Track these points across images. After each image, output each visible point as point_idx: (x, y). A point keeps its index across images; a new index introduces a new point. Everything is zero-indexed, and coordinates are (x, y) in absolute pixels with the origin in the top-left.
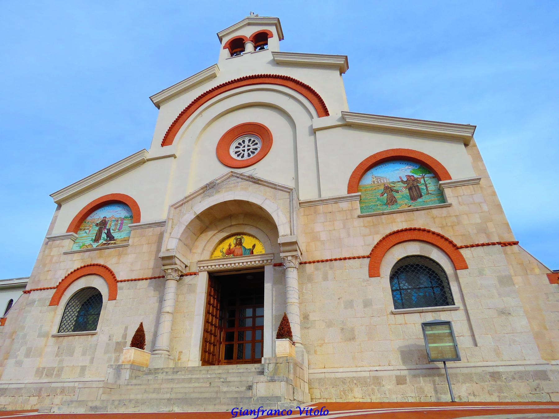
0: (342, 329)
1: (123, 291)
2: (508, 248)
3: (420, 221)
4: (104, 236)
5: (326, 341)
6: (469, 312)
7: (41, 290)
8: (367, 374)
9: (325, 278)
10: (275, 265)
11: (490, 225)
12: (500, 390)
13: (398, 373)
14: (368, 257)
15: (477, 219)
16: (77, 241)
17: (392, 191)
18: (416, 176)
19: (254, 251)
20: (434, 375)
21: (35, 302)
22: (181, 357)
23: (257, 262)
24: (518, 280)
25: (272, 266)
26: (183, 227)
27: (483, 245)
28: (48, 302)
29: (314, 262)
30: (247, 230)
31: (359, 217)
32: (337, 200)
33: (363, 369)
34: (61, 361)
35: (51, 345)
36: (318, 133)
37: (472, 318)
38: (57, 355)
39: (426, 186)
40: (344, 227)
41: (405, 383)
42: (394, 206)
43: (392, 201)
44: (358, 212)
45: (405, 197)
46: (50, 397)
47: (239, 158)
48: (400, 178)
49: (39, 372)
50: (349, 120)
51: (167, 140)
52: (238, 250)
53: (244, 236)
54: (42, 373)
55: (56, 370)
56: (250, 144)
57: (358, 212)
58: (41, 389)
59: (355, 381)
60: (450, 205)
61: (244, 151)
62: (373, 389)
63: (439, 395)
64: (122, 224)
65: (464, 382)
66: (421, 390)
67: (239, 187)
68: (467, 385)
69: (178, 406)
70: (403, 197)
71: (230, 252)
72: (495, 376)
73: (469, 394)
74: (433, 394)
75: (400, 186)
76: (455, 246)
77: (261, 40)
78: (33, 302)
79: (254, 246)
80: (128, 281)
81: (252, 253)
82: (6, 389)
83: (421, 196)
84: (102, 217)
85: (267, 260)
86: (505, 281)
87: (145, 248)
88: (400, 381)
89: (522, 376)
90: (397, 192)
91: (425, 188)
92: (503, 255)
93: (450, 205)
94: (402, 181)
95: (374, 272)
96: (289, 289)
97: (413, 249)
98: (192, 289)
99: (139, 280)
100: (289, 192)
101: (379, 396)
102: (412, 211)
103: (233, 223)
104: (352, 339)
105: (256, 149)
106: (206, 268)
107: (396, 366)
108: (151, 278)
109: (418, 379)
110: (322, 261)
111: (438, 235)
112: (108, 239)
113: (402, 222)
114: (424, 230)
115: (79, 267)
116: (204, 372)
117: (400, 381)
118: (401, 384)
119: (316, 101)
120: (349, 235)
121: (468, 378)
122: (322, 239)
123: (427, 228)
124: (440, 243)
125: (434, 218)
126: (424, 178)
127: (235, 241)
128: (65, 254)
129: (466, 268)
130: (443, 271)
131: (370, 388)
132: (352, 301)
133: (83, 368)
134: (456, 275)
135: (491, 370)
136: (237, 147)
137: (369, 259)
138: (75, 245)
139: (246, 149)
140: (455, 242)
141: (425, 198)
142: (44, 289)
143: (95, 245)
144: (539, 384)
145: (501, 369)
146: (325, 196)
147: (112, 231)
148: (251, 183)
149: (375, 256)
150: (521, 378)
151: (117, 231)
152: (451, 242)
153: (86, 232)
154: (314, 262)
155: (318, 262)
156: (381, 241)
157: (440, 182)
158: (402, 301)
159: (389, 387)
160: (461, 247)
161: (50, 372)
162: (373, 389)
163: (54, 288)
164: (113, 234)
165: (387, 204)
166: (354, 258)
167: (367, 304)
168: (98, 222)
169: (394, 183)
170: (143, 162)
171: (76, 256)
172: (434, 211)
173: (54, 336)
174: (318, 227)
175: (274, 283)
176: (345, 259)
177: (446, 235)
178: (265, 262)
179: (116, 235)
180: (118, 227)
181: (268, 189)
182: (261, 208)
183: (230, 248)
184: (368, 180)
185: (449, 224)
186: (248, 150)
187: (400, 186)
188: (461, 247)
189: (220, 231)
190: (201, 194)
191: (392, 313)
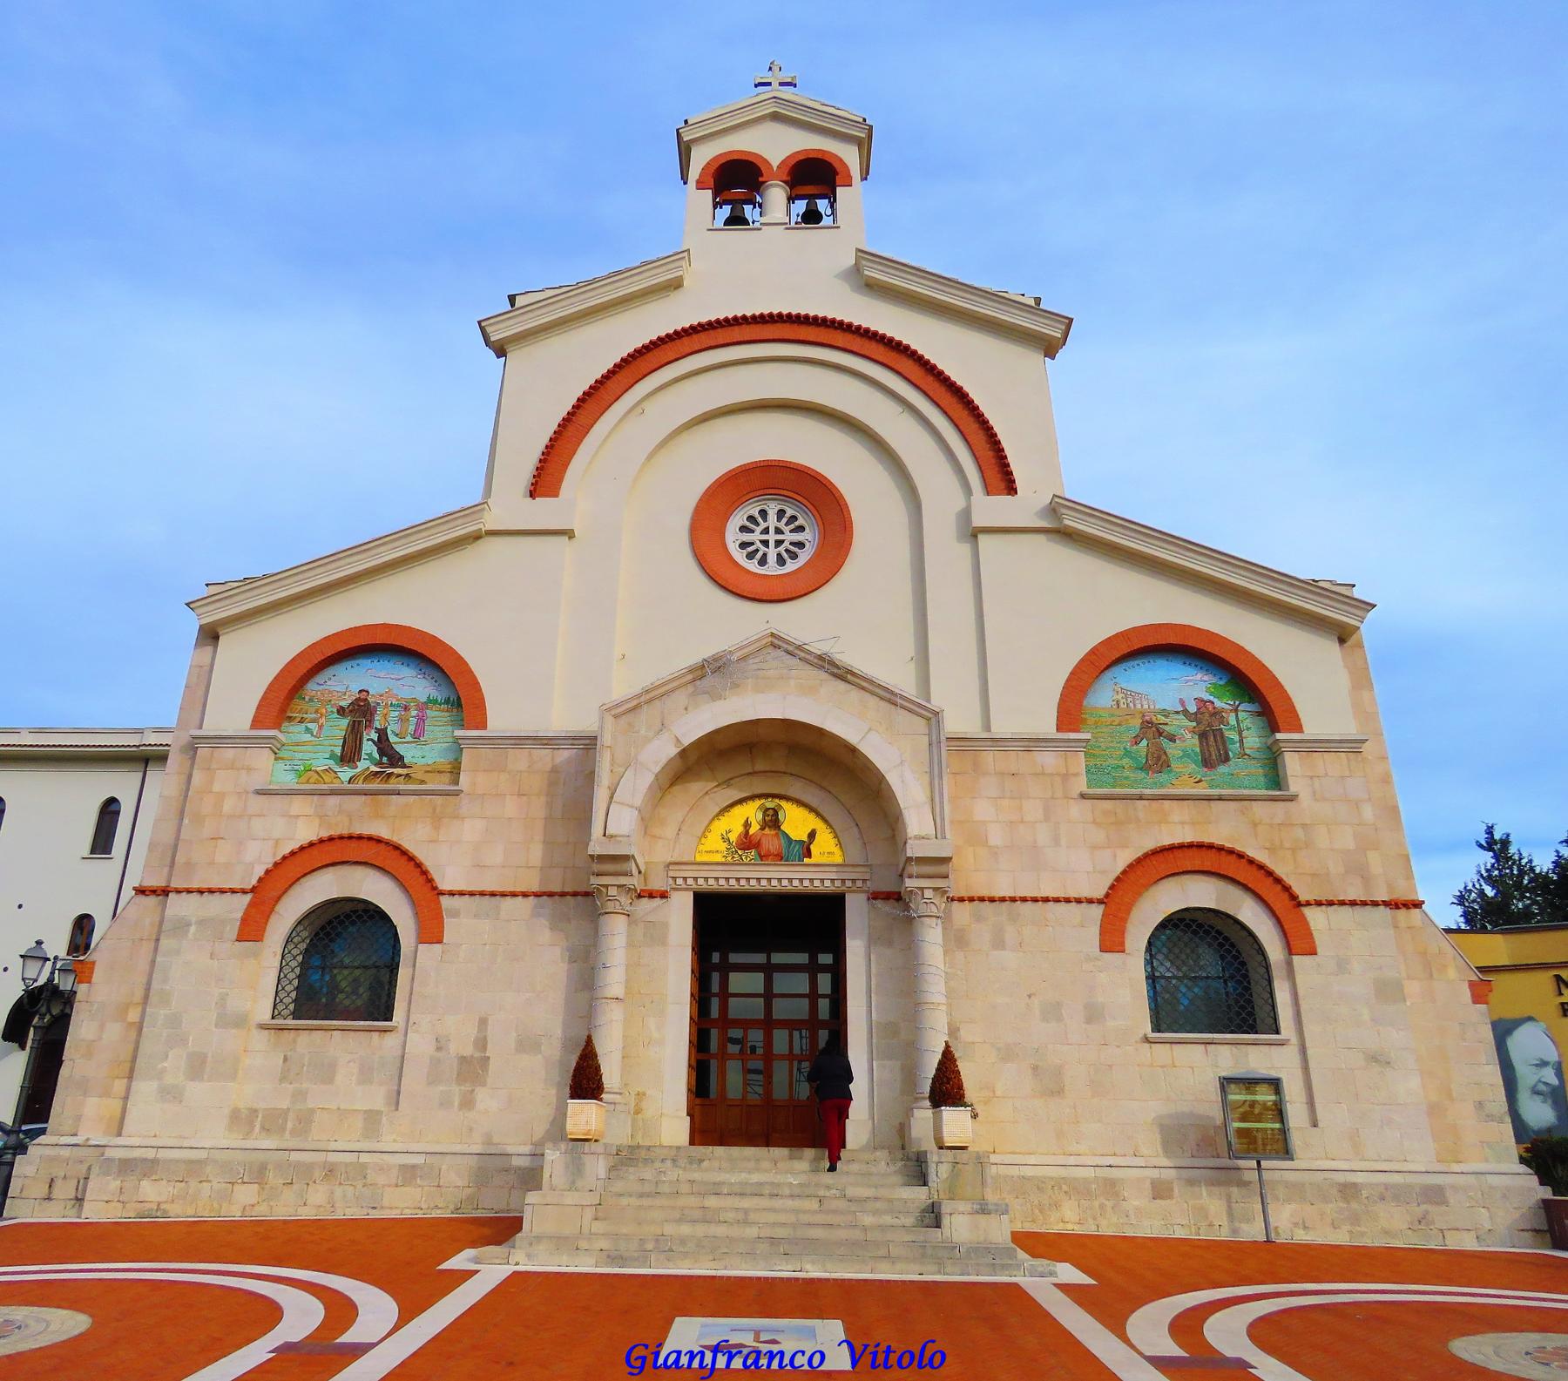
0: (1035, 1068)
1: (460, 921)
2: (1402, 912)
3: (1224, 827)
4: (369, 748)
5: (998, 1093)
6: (1309, 1052)
7: (201, 892)
8: (1089, 1173)
9: (999, 943)
10: (875, 896)
11: (1373, 858)
12: (1355, 1219)
13: (1155, 1173)
14: (1100, 902)
15: (1346, 840)
16: (281, 754)
17: (1160, 734)
18: (1218, 703)
19: (822, 853)
20: (1228, 1183)
21: (189, 925)
22: (644, 1105)
23: (828, 883)
24: (1413, 988)
25: (863, 897)
26: (650, 778)
27: (1353, 903)
28: (232, 930)
29: (971, 899)
30: (796, 788)
31: (1083, 796)
32: (1033, 743)
33: (1079, 1160)
34: (300, 1095)
35: (260, 1055)
36: (983, 539)
37: (1312, 1064)
38: (283, 1079)
39: (1240, 733)
40: (1047, 818)
41: (1170, 1197)
42: (1163, 777)
43: (1158, 762)
44: (1081, 784)
45: (1188, 756)
46: (295, 1187)
47: (752, 566)
48: (1182, 702)
49: (241, 1119)
50: (1070, 522)
51: (545, 480)
52: (771, 842)
53: (783, 803)
54: (251, 1124)
55: (291, 1116)
56: (782, 525)
57: (1081, 784)
58: (263, 1168)
59: (1065, 1188)
60: (1292, 798)
61: (765, 543)
62: (1102, 1206)
63: (1237, 1224)
64: (421, 719)
65: (1288, 1200)
66: (1202, 1212)
67: (792, 682)
68: (1293, 1206)
69: (813, 1263)
70: (1186, 755)
71: (747, 842)
72: (1349, 1191)
73: (1296, 1225)
74: (1225, 1223)
75: (1178, 725)
76: (1293, 897)
77: (815, 179)
78: (182, 926)
79: (812, 835)
80: (472, 894)
81: (809, 854)
82: (155, 1161)
83: (1227, 759)
84: (355, 688)
85: (854, 881)
86: (1388, 991)
87: (511, 807)
88: (1160, 1191)
89: (1395, 1194)
90: (1172, 739)
91: (1237, 738)
92: (1392, 932)
93: (1292, 798)
94: (1185, 712)
95: (1112, 940)
96: (926, 969)
97: (1200, 893)
98: (657, 934)
99: (503, 895)
100: (929, 719)
101: (1114, 1220)
102: (1209, 799)
103: (759, 766)
104: (1059, 1092)
105: (800, 545)
106: (690, 881)
107: (1149, 1158)
108: (537, 895)
109: (1196, 1189)
110: (992, 900)
111: (1261, 867)
112: (385, 759)
113: (1183, 823)
114: (1231, 852)
115: (314, 838)
116: (766, 1164)
117: (1160, 1191)
118: (1162, 1198)
119: (979, 438)
120: (1056, 841)
121: (1297, 1192)
122: (992, 842)
123: (1238, 848)
124: (1266, 888)
125: (1255, 825)
126: (1236, 711)
127: (760, 816)
128: (260, 792)
129: (1312, 952)
130: (1261, 951)
131: (1096, 1204)
132: (1059, 1005)
133: (372, 1120)
134: (1290, 964)
135: (1341, 1178)
136: (743, 529)
137: (1102, 907)
138: (280, 765)
139: (772, 537)
140: (1296, 889)
141: (1236, 765)
142: (211, 891)
143: (346, 773)
144: (1427, 1212)
145: (1359, 1178)
146: (1000, 728)
147: (392, 739)
148: (824, 676)
149: (1116, 901)
150: (1396, 1198)
151: (409, 738)
152: (1287, 889)
153: (308, 730)
154: (971, 899)
155: (982, 899)
156: (1131, 866)
157: (1279, 736)
158: (1170, 1014)
159: (1136, 1203)
160: (1308, 904)
161: (274, 1122)
162: (1102, 1206)
163: (244, 892)
164: (398, 748)
165: (1146, 768)
166: (1068, 900)
167: (1093, 1014)
168: (344, 704)
169: (1166, 713)
170: (476, 537)
171: (299, 805)
172: (1258, 809)
173: (263, 1027)
174: (983, 810)
175: (872, 941)
176: (1046, 900)
177: (1280, 871)
178: (848, 884)
179: (408, 752)
180: (412, 728)
181: (873, 702)
182: (853, 750)
183: (747, 832)
184: (1103, 696)
185: (1287, 845)
186: (766, 531)
187: (1178, 725)
188: (1308, 904)
189: (727, 783)
190: (685, 684)
191: (1146, 1040)
